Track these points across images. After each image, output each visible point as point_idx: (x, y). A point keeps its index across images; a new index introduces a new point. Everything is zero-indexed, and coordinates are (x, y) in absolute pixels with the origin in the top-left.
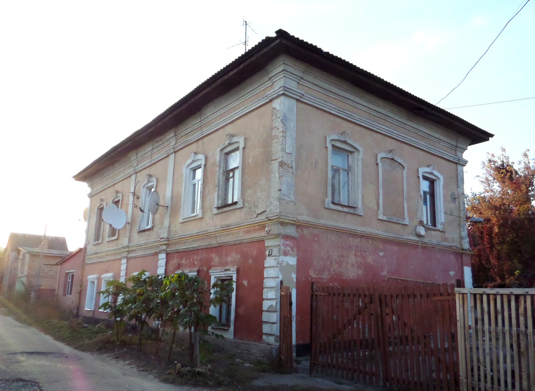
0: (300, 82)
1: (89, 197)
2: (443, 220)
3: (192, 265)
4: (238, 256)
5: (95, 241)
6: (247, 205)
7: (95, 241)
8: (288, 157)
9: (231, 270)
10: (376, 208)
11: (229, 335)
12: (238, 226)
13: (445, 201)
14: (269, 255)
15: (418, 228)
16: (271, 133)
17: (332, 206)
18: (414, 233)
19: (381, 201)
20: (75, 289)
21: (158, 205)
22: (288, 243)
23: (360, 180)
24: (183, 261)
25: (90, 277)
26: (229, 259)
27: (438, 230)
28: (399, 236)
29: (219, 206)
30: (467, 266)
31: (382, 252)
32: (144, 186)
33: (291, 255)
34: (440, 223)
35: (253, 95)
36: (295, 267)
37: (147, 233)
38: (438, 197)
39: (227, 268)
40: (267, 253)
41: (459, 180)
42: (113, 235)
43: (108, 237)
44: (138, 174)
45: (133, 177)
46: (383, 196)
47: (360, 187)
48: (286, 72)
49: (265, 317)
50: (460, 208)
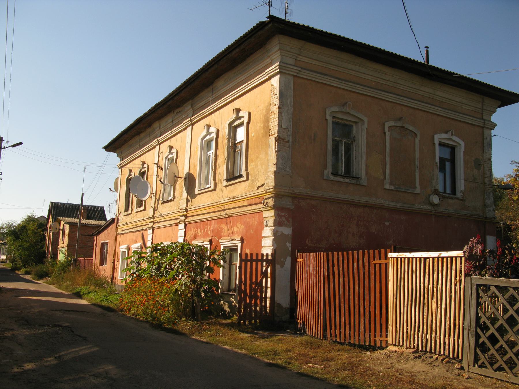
0: (298, 59)
2: (463, 188)
3: (206, 235)
4: (243, 226)
5: (125, 212)
6: (250, 177)
7: (125, 212)
8: (284, 132)
9: (237, 239)
10: (382, 177)
16: (269, 110)
17: (332, 178)
19: (388, 171)
20: (109, 259)
21: (176, 176)
22: (282, 214)
23: (364, 149)
24: (199, 231)
26: (235, 229)
29: (229, 178)
30: (491, 235)
32: (166, 158)
33: (286, 226)
37: (169, 204)
39: (233, 238)
40: (264, 223)
41: (485, 144)
42: (141, 206)
43: (136, 208)
44: (162, 145)
45: (157, 147)
47: (364, 157)
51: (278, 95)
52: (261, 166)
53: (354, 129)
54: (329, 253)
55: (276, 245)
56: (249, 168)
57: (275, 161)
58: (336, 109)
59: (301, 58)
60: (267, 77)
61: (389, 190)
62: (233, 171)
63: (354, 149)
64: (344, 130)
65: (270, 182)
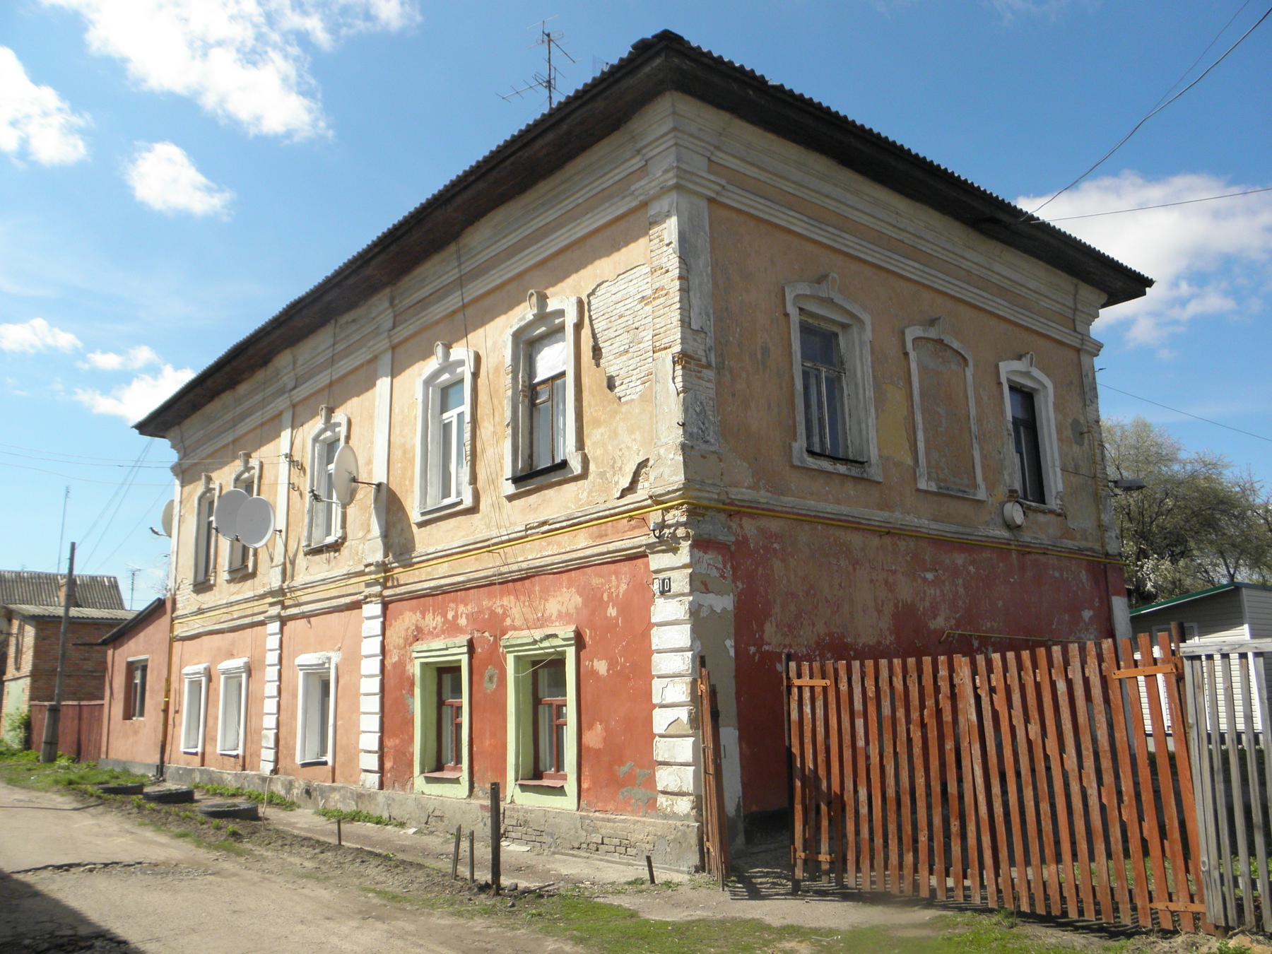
1: (176, 475)
2: (1060, 487)
3: (452, 628)
6: (592, 467)
8: (695, 340)
11: (568, 802)
12: (574, 524)
13: (1060, 440)
14: (663, 593)
15: (1008, 507)
17: (811, 462)
18: (999, 521)
19: (921, 445)
20: (153, 702)
21: (354, 480)
23: (870, 393)
25: (188, 669)
27: (1052, 512)
28: (968, 530)
29: (519, 474)
32: (315, 440)
33: (719, 593)
34: (1054, 493)
36: (731, 617)
38: (1045, 430)
39: (550, 631)
41: (1087, 389)
46: (925, 431)
47: (873, 410)
48: (679, 135)
49: (662, 750)
51: (675, 244)
55: (698, 643)
56: (588, 442)
57: (678, 416)
58: (804, 289)
59: (721, 157)
61: (926, 492)
62: (531, 456)
64: (822, 343)
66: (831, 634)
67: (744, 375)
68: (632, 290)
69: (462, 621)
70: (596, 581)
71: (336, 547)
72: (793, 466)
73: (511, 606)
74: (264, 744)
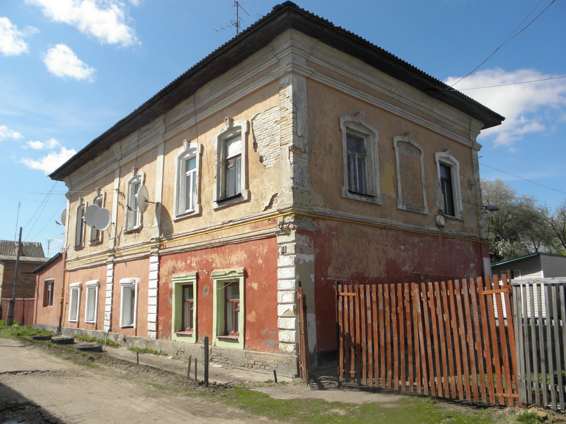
0: (309, 59)
1: (68, 197)
2: (461, 209)
3: (189, 268)
6: (252, 197)
8: (299, 141)
10: (394, 196)
11: (239, 346)
12: (244, 222)
13: (462, 188)
14: (283, 253)
17: (350, 196)
18: (434, 223)
19: (400, 189)
20: (56, 299)
21: (147, 201)
23: (377, 166)
27: (457, 220)
29: (220, 199)
31: (403, 245)
32: (130, 183)
34: (459, 212)
35: (255, 73)
36: (313, 264)
39: (232, 270)
41: (474, 165)
46: (402, 183)
48: (294, 48)
49: (281, 323)
50: (477, 195)
51: (291, 97)
52: (270, 181)
53: (365, 142)
54: (385, 285)
55: (298, 276)
56: (251, 186)
57: (291, 174)
59: (312, 59)
60: (273, 79)
61: (401, 210)
62: (225, 191)
63: (366, 165)
64: (356, 143)
65: (286, 200)
66: (358, 273)
67: (321, 156)
68: (272, 118)
69: (194, 265)
70: (253, 248)
71: (138, 231)
72: (342, 198)
73: (215, 258)
74: (105, 318)
